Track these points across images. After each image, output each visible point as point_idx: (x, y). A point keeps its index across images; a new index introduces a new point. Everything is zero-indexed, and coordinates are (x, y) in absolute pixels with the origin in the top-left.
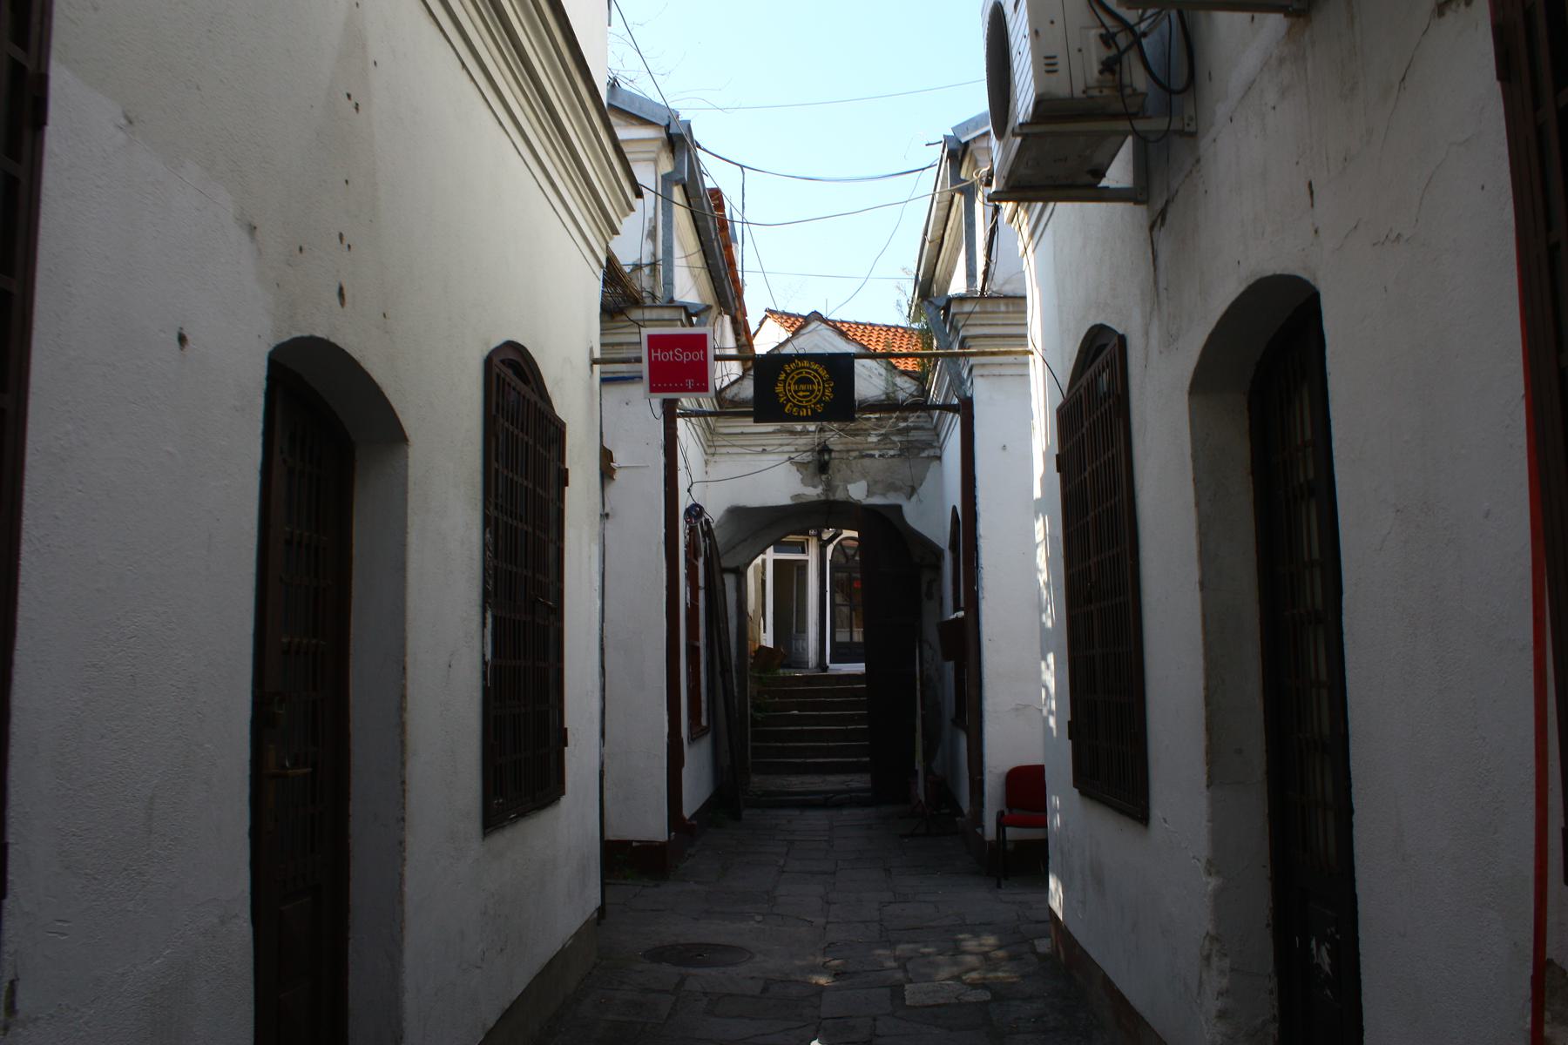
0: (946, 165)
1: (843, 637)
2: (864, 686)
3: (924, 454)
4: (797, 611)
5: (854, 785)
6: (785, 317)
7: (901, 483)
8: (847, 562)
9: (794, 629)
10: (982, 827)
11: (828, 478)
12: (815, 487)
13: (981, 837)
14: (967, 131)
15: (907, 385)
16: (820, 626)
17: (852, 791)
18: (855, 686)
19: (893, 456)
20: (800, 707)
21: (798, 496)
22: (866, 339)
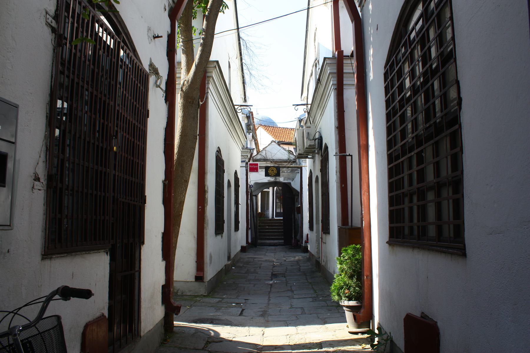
0: (298, 122)
1: (278, 211)
2: (282, 218)
3: (296, 172)
4: (267, 204)
5: (280, 242)
6: (264, 127)
8: (280, 192)
9: (424, 113)
10: (303, 244)
12: (273, 178)
13: (303, 246)
14: (302, 117)
15: (293, 157)
16: (419, 18)
17: (280, 243)
19: (289, 172)
21: (269, 180)
22: (286, 133)
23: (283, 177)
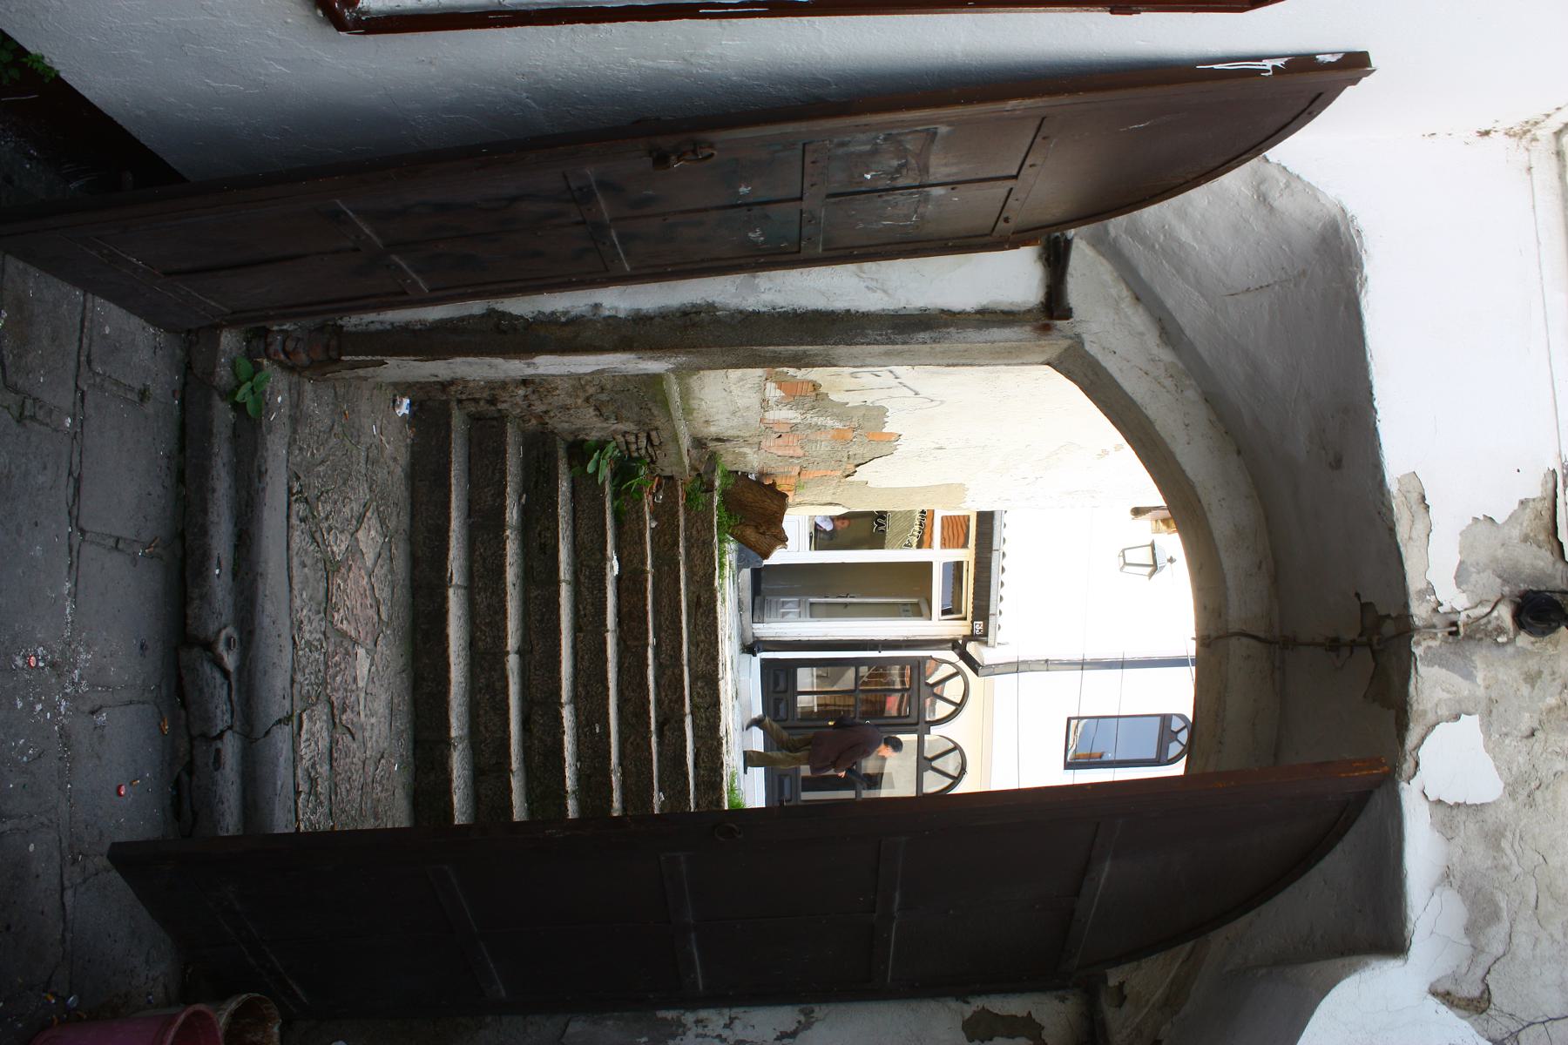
1: (806, 679)
4: (846, 605)
7: (1497, 948)
11: (1500, 630)
12: (1461, 577)
18: (688, 721)
20: (630, 583)
23: (1511, 790)
